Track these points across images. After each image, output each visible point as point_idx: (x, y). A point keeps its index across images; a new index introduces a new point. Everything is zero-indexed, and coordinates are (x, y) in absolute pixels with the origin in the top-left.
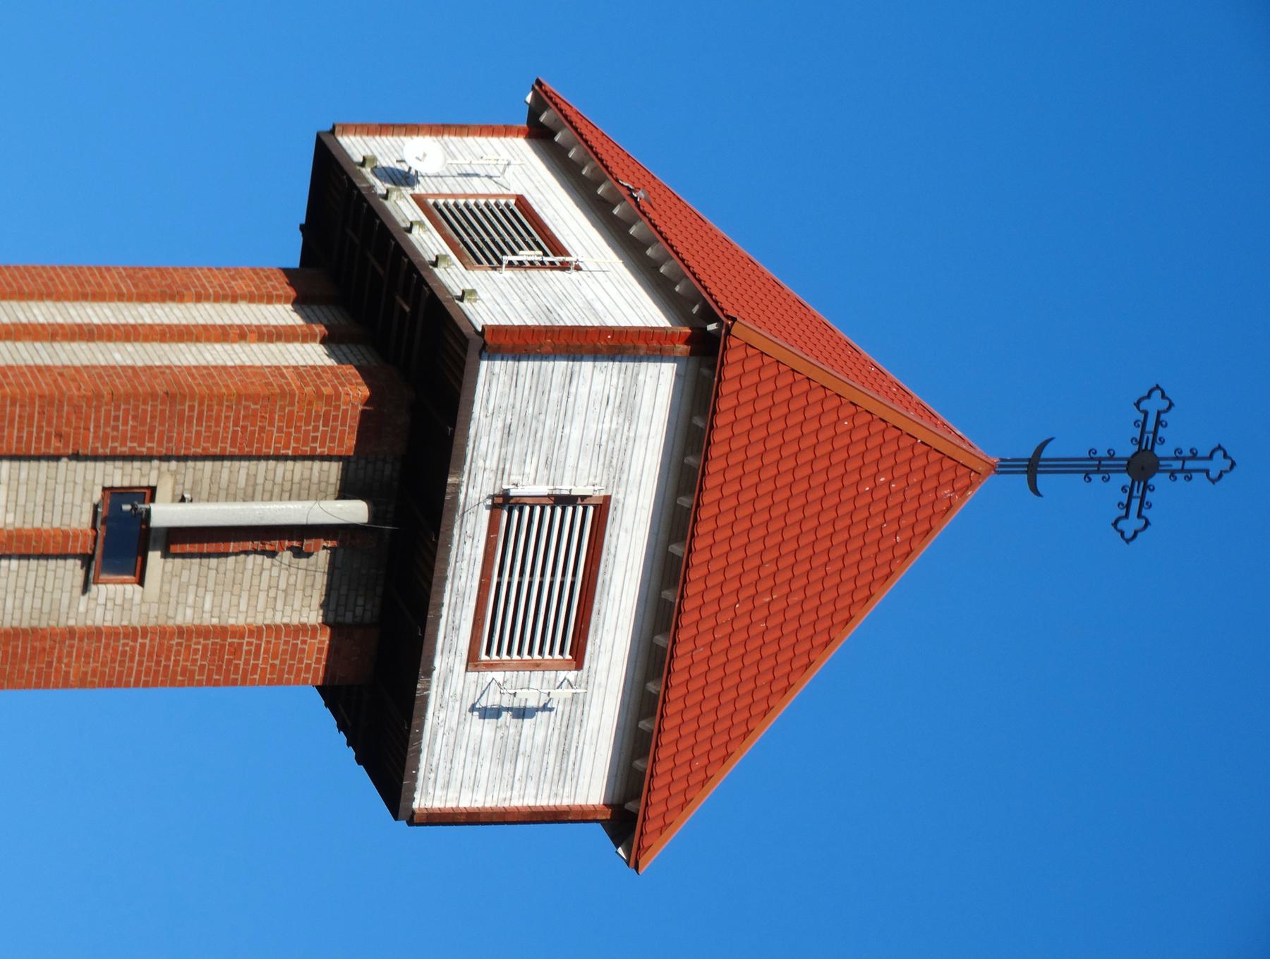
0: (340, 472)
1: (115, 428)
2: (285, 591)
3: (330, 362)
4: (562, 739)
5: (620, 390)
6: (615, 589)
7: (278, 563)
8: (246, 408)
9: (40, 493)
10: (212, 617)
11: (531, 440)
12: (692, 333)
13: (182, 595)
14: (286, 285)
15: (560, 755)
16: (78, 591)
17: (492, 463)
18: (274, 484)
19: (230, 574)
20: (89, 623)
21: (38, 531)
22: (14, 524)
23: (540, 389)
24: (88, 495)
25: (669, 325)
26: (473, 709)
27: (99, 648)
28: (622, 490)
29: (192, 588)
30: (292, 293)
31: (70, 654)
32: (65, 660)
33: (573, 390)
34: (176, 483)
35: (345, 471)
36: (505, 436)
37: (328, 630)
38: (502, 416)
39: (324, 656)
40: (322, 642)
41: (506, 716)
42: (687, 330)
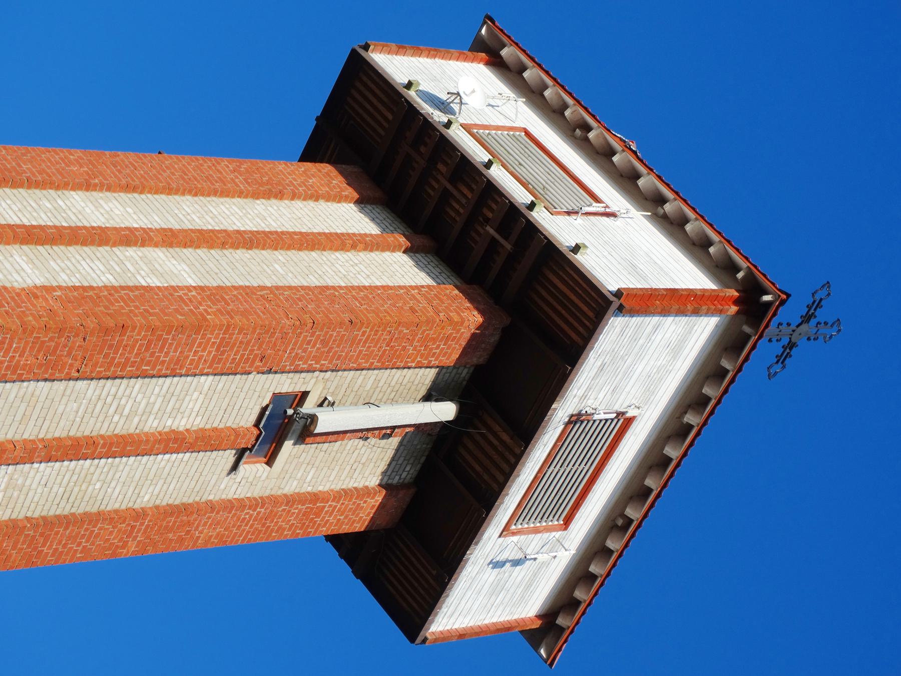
0: (435, 375)
1: (305, 351)
2: (364, 464)
3: (428, 281)
4: (532, 577)
5: (679, 337)
6: (610, 475)
7: (368, 444)
8: (400, 332)
9: (227, 400)
10: (309, 486)
11: (613, 374)
12: (739, 297)
13: (296, 471)
14: (346, 185)
15: (526, 587)
16: (226, 472)
17: (581, 392)
18: (389, 386)
19: (333, 454)
20: (224, 497)
21: (215, 430)
22: (198, 425)
23: (635, 337)
24: (260, 400)
25: (714, 287)
26: (491, 562)
27: (228, 517)
28: (646, 407)
29: (304, 466)
30: (356, 196)
31: (206, 523)
32: (200, 528)
33: (653, 338)
34: (324, 388)
35: (438, 374)
36: (599, 371)
37: (384, 492)
38: (603, 357)
39: (373, 511)
40: (377, 501)
41: (508, 565)
42: (736, 294)
